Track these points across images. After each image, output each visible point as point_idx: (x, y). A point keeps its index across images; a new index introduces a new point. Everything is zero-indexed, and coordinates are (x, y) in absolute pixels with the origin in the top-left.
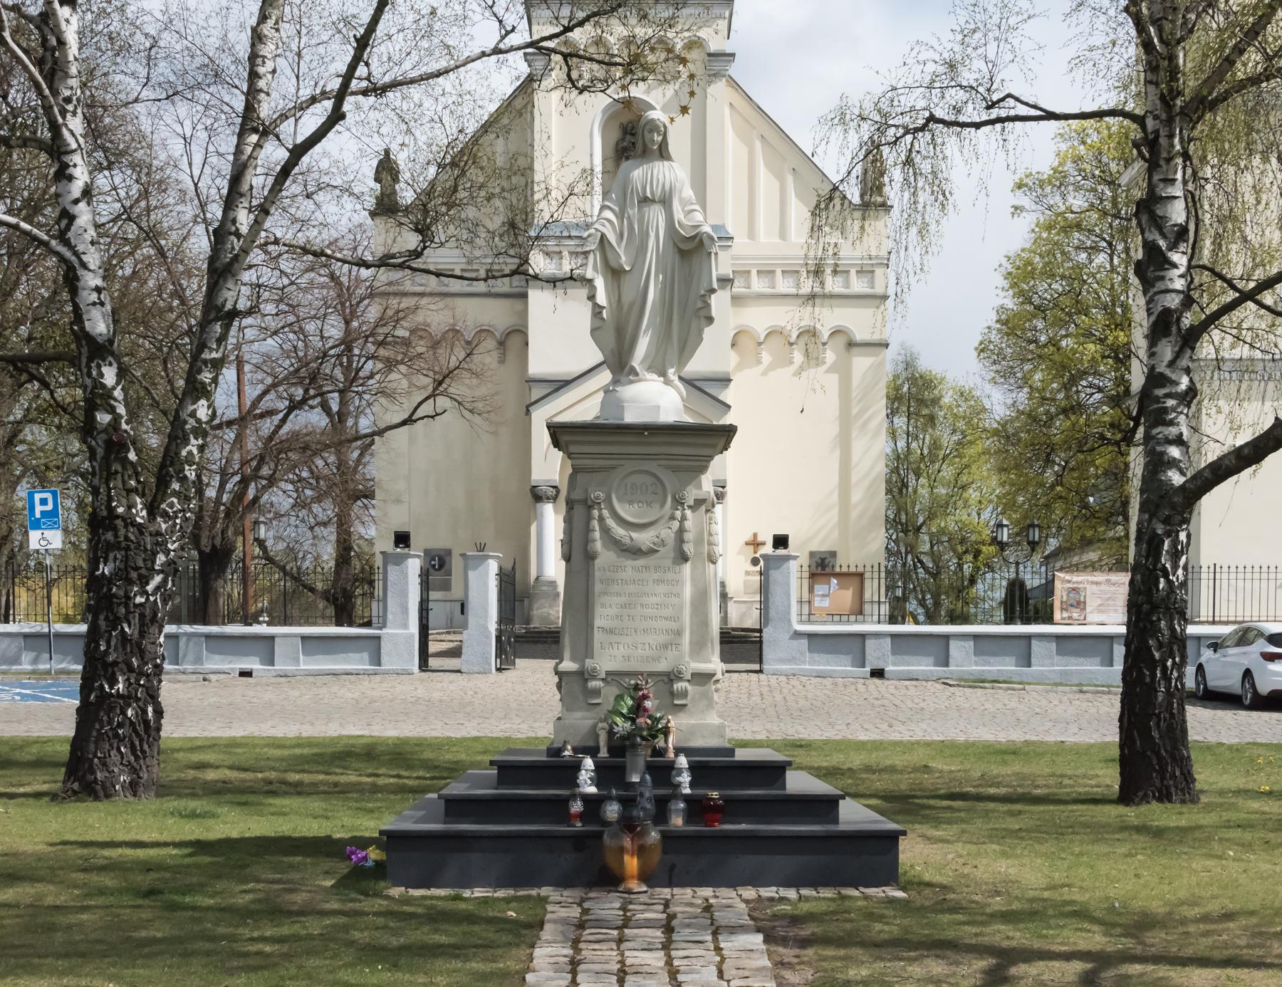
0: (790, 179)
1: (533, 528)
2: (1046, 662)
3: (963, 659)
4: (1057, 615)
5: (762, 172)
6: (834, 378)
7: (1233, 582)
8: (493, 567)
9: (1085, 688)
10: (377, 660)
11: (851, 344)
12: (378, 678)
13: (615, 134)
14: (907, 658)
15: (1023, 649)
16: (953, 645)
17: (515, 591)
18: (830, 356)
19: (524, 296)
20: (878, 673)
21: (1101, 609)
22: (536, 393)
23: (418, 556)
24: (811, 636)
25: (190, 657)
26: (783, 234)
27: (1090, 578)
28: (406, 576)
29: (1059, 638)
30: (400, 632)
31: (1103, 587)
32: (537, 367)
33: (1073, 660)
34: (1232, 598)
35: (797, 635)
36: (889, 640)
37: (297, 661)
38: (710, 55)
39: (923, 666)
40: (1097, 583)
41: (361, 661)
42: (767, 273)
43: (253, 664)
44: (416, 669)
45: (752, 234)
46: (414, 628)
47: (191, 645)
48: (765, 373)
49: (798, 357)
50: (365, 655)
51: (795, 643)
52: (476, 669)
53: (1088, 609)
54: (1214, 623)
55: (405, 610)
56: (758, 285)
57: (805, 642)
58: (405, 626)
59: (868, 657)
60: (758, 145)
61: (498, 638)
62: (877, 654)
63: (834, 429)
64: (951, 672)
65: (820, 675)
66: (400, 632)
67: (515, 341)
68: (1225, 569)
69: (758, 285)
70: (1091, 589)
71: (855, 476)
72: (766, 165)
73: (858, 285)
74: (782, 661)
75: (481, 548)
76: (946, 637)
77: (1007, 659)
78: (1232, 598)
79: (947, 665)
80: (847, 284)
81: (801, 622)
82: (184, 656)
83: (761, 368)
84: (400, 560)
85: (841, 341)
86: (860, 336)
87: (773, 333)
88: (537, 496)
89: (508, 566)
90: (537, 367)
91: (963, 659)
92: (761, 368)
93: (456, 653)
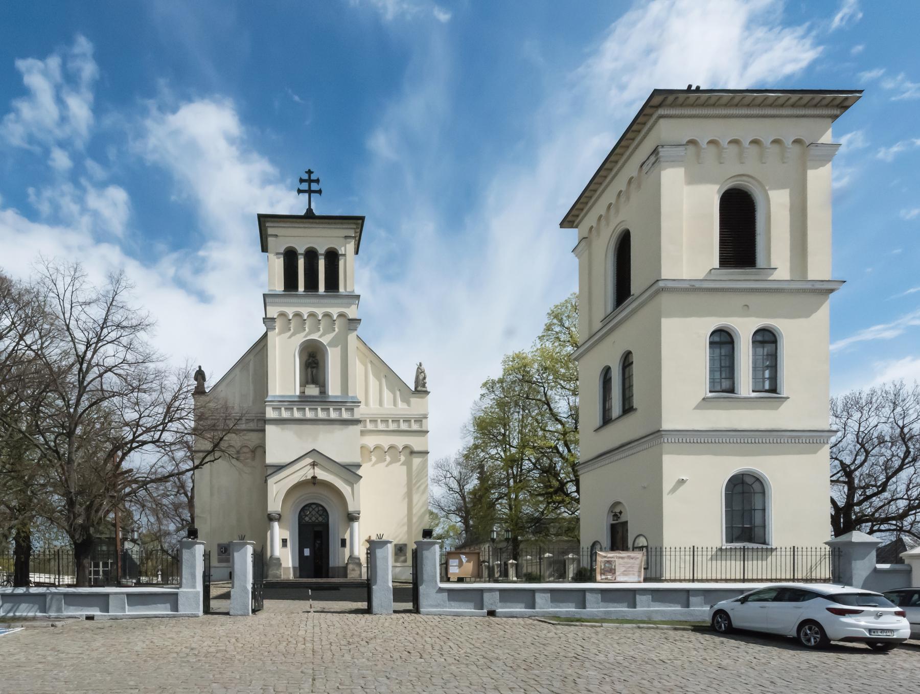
0: (384, 380)
1: (269, 533)
2: (594, 608)
3: (543, 605)
4: (599, 578)
5: (371, 377)
6: (405, 468)
7: (683, 557)
8: (250, 550)
9: (641, 625)
10: (175, 608)
11: (412, 453)
12: (173, 621)
13: (305, 358)
14: (508, 604)
15: (580, 598)
16: (538, 595)
17: (262, 562)
18: (403, 458)
19: (264, 431)
20: (492, 613)
21: (625, 573)
22: (269, 472)
23: (203, 544)
24: (450, 591)
25: (54, 608)
26: (381, 403)
27: (618, 555)
28: (194, 556)
29: (603, 591)
30: (191, 589)
31: (626, 560)
32: (270, 459)
33: (611, 604)
34: (682, 566)
35: (441, 590)
36: (498, 593)
37: (123, 609)
38: (350, 320)
39: (519, 609)
40: (622, 558)
41: (166, 610)
42: (374, 421)
43: (96, 612)
44: (201, 613)
45: (367, 404)
46: (200, 588)
47: (54, 601)
48: (373, 465)
49: (388, 459)
50: (168, 606)
51: (440, 595)
52: (239, 613)
53: (617, 573)
54: (693, 581)
55: (193, 576)
56: (370, 426)
57: (446, 594)
58: (194, 586)
59: (485, 603)
60: (369, 365)
61: (253, 593)
62: (490, 601)
63: (405, 490)
64: (537, 612)
65: (457, 615)
66: (191, 589)
67: (259, 451)
68: (700, 549)
69: (370, 426)
70: (618, 562)
71: (414, 511)
72: (374, 375)
73: (415, 427)
74: (432, 606)
75: (242, 538)
76: (533, 591)
77: (570, 604)
78: (682, 566)
79: (534, 607)
80: (410, 426)
81: (441, 581)
82: (50, 607)
83: (372, 463)
84: (190, 546)
85: (408, 451)
86: (416, 449)
87: (377, 447)
88: (271, 518)
89: (259, 549)
90: (270, 459)
91: (543, 605)
92: (372, 463)
93: (227, 596)
